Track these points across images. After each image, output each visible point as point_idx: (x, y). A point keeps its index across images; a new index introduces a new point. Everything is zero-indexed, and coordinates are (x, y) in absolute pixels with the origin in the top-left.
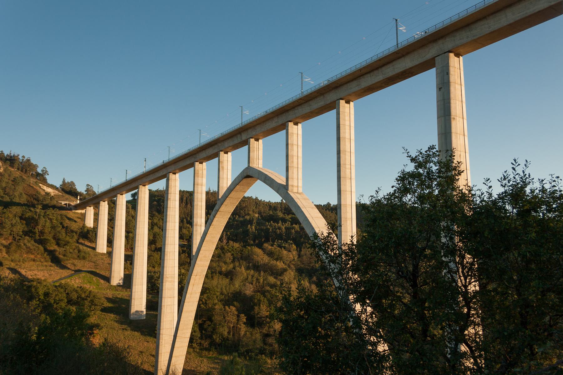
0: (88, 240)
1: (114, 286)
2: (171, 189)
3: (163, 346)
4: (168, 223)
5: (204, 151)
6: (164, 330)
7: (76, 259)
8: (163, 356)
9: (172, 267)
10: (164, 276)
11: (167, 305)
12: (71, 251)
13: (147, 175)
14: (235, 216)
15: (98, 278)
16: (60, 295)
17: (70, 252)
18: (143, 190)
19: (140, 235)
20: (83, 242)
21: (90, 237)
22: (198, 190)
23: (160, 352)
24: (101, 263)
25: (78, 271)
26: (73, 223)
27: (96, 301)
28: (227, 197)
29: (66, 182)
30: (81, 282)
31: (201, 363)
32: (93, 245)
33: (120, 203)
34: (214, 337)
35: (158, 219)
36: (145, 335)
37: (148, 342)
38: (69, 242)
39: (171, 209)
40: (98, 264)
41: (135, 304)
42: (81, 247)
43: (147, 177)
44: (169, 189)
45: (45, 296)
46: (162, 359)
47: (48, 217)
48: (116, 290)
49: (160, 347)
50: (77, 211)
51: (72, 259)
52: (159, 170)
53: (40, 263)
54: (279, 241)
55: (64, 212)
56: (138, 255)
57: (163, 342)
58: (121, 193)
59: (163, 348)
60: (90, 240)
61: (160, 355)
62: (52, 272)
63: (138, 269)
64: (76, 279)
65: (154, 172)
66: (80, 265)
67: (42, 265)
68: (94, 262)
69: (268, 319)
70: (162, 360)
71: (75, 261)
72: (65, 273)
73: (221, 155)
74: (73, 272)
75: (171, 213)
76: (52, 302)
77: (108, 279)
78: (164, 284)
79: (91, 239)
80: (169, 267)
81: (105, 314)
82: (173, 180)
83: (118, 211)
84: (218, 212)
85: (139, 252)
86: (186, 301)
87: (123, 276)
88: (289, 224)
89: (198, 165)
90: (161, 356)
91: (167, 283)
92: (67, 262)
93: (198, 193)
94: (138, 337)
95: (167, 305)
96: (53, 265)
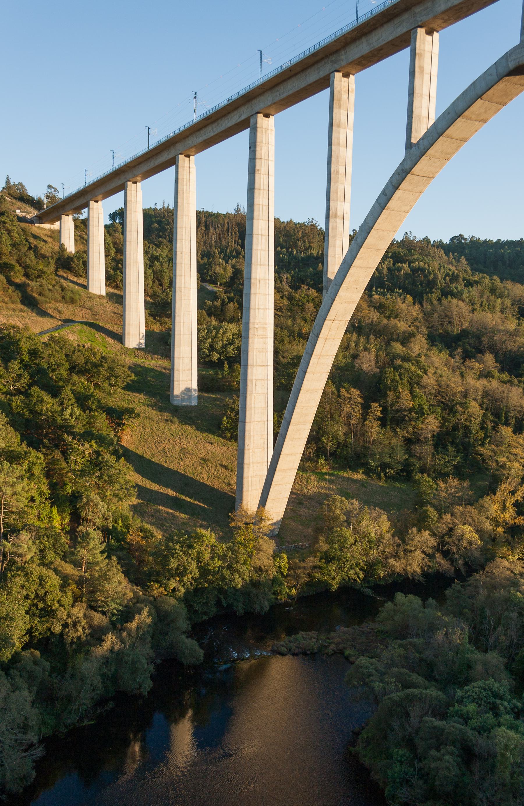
0: (71, 272)
1: (132, 350)
2: (261, 149)
3: (251, 451)
4: (255, 222)
5: (364, 39)
6: (252, 424)
7: (60, 302)
8: (251, 469)
9: (264, 309)
10: (251, 326)
11: (256, 380)
12: (50, 287)
13: (199, 130)
14: (290, 250)
15: (103, 335)
16: (57, 356)
17: (50, 290)
18: (185, 165)
19: (183, 253)
20: (65, 275)
21: (75, 266)
22: (338, 138)
23: (246, 461)
24: (102, 312)
25: (68, 322)
26: (42, 243)
27: (120, 371)
28: (441, 135)
29: (12, 182)
30: (76, 339)
31: (307, 482)
32: (82, 281)
33: (133, 200)
34: (324, 440)
35: (167, 249)
36: (202, 431)
37: (212, 444)
38: (44, 273)
39: (261, 192)
40: (96, 312)
41: (181, 379)
42: (64, 282)
43: (198, 133)
44: (258, 149)
45: (32, 357)
46: (250, 472)
47: (4, 226)
48: (136, 356)
49: (246, 452)
50: (43, 226)
51: (53, 302)
52: (229, 113)
53: (4, 304)
54: (379, 289)
55: (23, 225)
56: (181, 291)
57: (251, 445)
58: (134, 180)
59: (251, 454)
60: (75, 273)
61: (245, 467)
62: (27, 320)
63: (182, 317)
64: (68, 333)
65: (217, 120)
66: (68, 311)
67: (8, 308)
68: (90, 309)
69: (413, 414)
70: (250, 475)
71: (59, 305)
72: (48, 323)
73: (418, 37)
74: (60, 323)
75: (261, 200)
76: (45, 366)
77: (120, 338)
78: (250, 340)
79: (76, 271)
80: (258, 309)
81: (130, 393)
82: (264, 130)
83: (131, 214)
84: (409, 175)
85: (183, 286)
86: (308, 371)
87: (144, 333)
88: (389, 261)
89: (341, 81)
90: (248, 468)
91: (256, 340)
92: (46, 306)
93: (338, 144)
94: (194, 435)
95: (256, 380)
96: (25, 308)
